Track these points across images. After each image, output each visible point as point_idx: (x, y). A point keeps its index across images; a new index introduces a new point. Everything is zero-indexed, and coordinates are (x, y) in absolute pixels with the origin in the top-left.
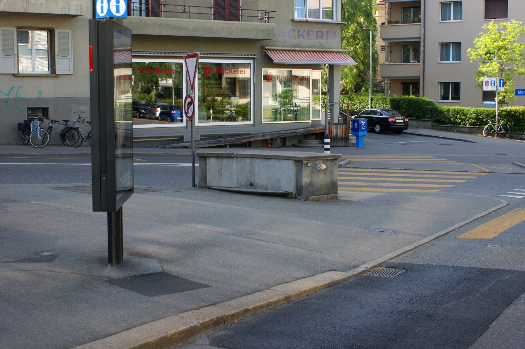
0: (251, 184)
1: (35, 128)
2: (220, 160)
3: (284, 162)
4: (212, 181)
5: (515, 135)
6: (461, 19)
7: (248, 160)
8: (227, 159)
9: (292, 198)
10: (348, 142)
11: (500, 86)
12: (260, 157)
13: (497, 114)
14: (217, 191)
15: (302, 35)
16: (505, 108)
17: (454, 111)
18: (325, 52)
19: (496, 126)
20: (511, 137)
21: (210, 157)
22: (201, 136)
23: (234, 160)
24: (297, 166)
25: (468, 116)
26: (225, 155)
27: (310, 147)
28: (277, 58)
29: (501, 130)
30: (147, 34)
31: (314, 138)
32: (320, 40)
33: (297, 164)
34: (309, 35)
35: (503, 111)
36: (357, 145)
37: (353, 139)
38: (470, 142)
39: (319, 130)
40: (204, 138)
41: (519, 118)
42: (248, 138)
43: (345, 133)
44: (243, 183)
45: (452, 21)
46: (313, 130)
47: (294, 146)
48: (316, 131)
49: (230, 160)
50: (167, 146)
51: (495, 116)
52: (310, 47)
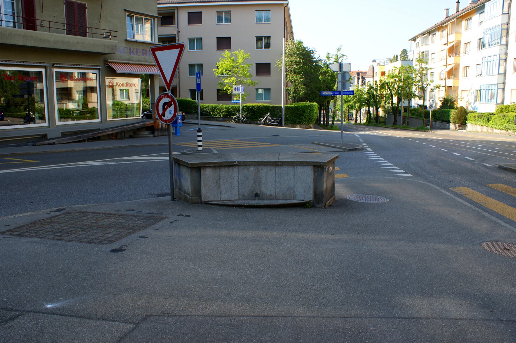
0: (257, 195)
2: (217, 170)
3: (299, 169)
6: (202, 49)
7: (252, 169)
8: (227, 169)
9: (311, 207)
15: (132, 52)
16: (245, 105)
17: (212, 107)
18: (149, 65)
20: (250, 123)
21: (205, 167)
22: (62, 133)
23: (235, 169)
24: (315, 172)
26: (225, 164)
28: (119, 69)
29: (244, 118)
30: (12, 43)
32: (144, 56)
34: (137, 52)
36: (176, 134)
37: (173, 130)
40: (65, 135)
42: (101, 133)
44: (246, 194)
45: (196, 50)
47: (131, 137)
50: (37, 144)
52: (138, 61)
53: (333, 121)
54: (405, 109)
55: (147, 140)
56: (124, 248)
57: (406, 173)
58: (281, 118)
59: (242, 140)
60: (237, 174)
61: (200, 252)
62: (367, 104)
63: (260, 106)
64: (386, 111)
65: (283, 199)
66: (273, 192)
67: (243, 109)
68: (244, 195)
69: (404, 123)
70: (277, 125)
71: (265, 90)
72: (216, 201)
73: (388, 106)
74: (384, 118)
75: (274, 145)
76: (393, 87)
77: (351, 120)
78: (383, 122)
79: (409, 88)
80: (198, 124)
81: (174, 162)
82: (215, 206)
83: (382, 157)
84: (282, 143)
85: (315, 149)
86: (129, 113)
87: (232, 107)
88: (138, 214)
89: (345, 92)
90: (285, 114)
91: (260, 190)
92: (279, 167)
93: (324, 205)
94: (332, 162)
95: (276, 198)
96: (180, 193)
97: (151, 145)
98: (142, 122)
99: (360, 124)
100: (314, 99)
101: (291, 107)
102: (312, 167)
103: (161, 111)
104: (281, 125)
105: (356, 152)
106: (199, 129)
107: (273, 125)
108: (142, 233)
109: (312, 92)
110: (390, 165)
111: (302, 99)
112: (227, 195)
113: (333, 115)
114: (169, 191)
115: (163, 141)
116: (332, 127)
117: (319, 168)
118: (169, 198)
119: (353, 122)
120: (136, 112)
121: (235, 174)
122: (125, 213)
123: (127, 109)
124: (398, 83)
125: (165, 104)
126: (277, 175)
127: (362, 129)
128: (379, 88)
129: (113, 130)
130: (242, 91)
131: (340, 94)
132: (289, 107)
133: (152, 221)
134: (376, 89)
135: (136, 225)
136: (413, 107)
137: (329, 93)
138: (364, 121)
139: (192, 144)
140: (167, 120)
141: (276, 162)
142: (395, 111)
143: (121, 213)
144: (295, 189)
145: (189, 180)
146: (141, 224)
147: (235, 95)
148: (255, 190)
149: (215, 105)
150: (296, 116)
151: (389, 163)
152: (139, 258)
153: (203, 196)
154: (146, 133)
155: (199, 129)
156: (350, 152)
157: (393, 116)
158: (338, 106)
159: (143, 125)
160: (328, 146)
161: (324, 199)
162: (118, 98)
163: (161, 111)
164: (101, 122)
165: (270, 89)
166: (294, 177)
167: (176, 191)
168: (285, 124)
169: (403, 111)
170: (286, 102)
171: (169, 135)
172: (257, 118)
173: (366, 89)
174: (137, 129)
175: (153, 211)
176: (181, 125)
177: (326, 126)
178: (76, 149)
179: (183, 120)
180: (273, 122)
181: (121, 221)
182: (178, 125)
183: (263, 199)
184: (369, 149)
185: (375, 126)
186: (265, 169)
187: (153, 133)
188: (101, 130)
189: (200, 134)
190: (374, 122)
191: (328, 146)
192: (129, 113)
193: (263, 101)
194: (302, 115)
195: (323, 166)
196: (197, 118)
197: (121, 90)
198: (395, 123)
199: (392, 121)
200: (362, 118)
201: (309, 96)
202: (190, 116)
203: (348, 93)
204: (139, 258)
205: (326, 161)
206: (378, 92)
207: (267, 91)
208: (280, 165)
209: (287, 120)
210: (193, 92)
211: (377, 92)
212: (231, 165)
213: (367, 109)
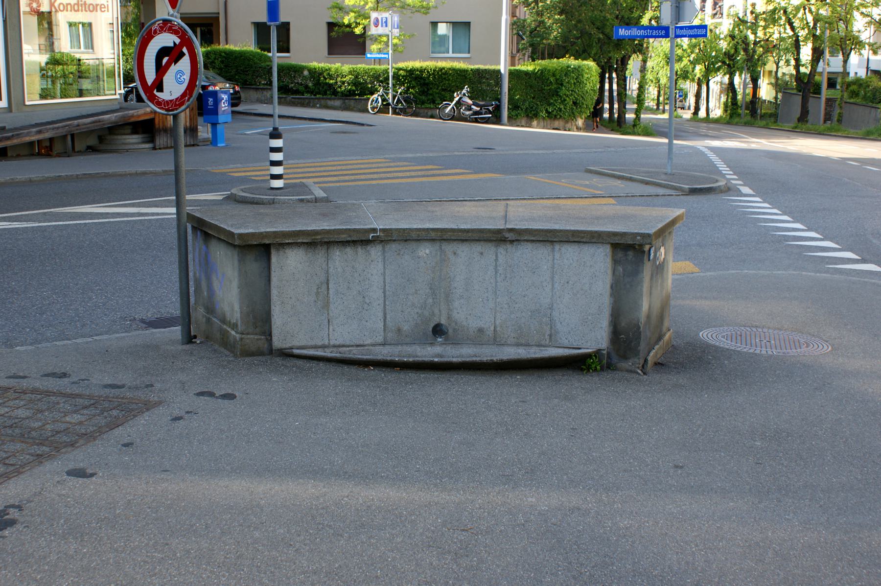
0: (438, 330)
2: (321, 253)
3: (569, 253)
4: (291, 327)
5: (422, 111)
7: (425, 251)
8: (349, 250)
9: (602, 369)
10: (197, 136)
11: (705, 36)
12: (476, 236)
13: (391, 74)
16: (401, 65)
19: (390, 96)
21: (282, 245)
23: (375, 251)
24: (615, 262)
25: (339, 79)
26: (344, 237)
27: (127, 151)
29: (399, 101)
31: (129, 131)
33: (620, 254)
35: (401, 69)
36: (214, 141)
38: (363, 125)
39: (145, 114)
41: (427, 81)
42: (8, 138)
43: (190, 119)
44: (406, 327)
46: (133, 116)
47: (92, 149)
48: (139, 116)
49: (359, 249)
51: (387, 79)
53: (637, 112)
54: (829, 79)
55: (137, 159)
56: (13, 514)
57: (864, 261)
58: (499, 100)
59: (394, 160)
61: (257, 534)
62: (729, 65)
63: (441, 69)
64: (779, 85)
65: (518, 345)
66: (486, 322)
67: (396, 76)
68: (399, 330)
69: (828, 117)
70: (487, 121)
71: (455, 24)
72: (315, 347)
73: (787, 70)
74: (775, 104)
75: (481, 176)
76: (802, 20)
77: (683, 108)
78: (771, 115)
79: (847, 22)
80: (271, 116)
81: (193, 228)
82: (314, 364)
83: (785, 213)
84: (504, 171)
85: (597, 188)
86: (86, 84)
87: (366, 72)
88: (76, 390)
89: (681, 28)
90: (509, 90)
91: (449, 317)
92: (509, 246)
93: (642, 361)
94: (664, 232)
95: (496, 341)
96: (208, 320)
97: (144, 174)
98: (121, 109)
99: (707, 119)
100: (584, 51)
101: (526, 73)
102: (608, 249)
103: (150, 75)
104: (497, 120)
105: (711, 197)
106: (275, 129)
107: (476, 121)
108: (77, 458)
109: (583, 33)
110: (812, 238)
111: (555, 52)
112: (353, 327)
113: (639, 96)
114: (174, 309)
115: (162, 162)
116: (635, 128)
117: (631, 252)
118: (176, 332)
119: (687, 115)
120: (106, 84)
121: (372, 264)
122: (37, 384)
123: (81, 75)
124: (813, 8)
125: (163, 52)
127: (711, 133)
128: (762, 23)
129: (40, 132)
130: (393, 27)
131: (667, 36)
132: (519, 72)
133: (115, 413)
134: (754, 27)
135: (63, 426)
136: (852, 75)
137: (634, 32)
138: (717, 112)
139: (256, 171)
140: (168, 102)
141: (499, 231)
142: (806, 86)
143: (24, 383)
144: (555, 314)
145: (235, 284)
146: (81, 423)
147: (376, 39)
148: (433, 314)
149: (322, 65)
150: (539, 98)
151: (809, 229)
152: (53, 557)
153: (275, 332)
154: (134, 139)
155: (275, 129)
157: (798, 99)
158: (653, 68)
159: (123, 117)
160: (631, 179)
161: (643, 346)
162: (64, 44)
163: (150, 75)
164: (10, 109)
165: (468, 24)
166: (552, 278)
167: (199, 314)
168: (509, 117)
169: (825, 85)
170: (513, 60)
171: (175, 147)
172: (434, 102)
173: (725, 26)
174: (109, 128)
175: (125, 378)
176: (229, 118)
177: (618, 125)
179: (233, 105)
180: (476, 113)
181: (22, 413)
182: (221, 118)
183: (456, 343)
184: (746, 190)
185: (746, 124)
186: (465, 251)
187: (152, 140)
188: (11, 130)
189: (277, 143)
190: (745, 113)
191: (631, 179)
192: (86, 84)
193: (451, 54)
194: (556, 93)
195: (641, 246)
196: (270, 101)
197: (71, 25)
198: (803, 117)
199: (797, 112)
200: (711, 105)
201: (573, 44)
202: (253, 95)
203: (691, 32)
204: (53, 557)
205: (652, 231)
206: (760, 34)
207: (462, 27)
208: (512, 242)
209: (514, 106)
210: (262, 31)
211: (755, 34)
212: (361, 240)
213: (726, 79)
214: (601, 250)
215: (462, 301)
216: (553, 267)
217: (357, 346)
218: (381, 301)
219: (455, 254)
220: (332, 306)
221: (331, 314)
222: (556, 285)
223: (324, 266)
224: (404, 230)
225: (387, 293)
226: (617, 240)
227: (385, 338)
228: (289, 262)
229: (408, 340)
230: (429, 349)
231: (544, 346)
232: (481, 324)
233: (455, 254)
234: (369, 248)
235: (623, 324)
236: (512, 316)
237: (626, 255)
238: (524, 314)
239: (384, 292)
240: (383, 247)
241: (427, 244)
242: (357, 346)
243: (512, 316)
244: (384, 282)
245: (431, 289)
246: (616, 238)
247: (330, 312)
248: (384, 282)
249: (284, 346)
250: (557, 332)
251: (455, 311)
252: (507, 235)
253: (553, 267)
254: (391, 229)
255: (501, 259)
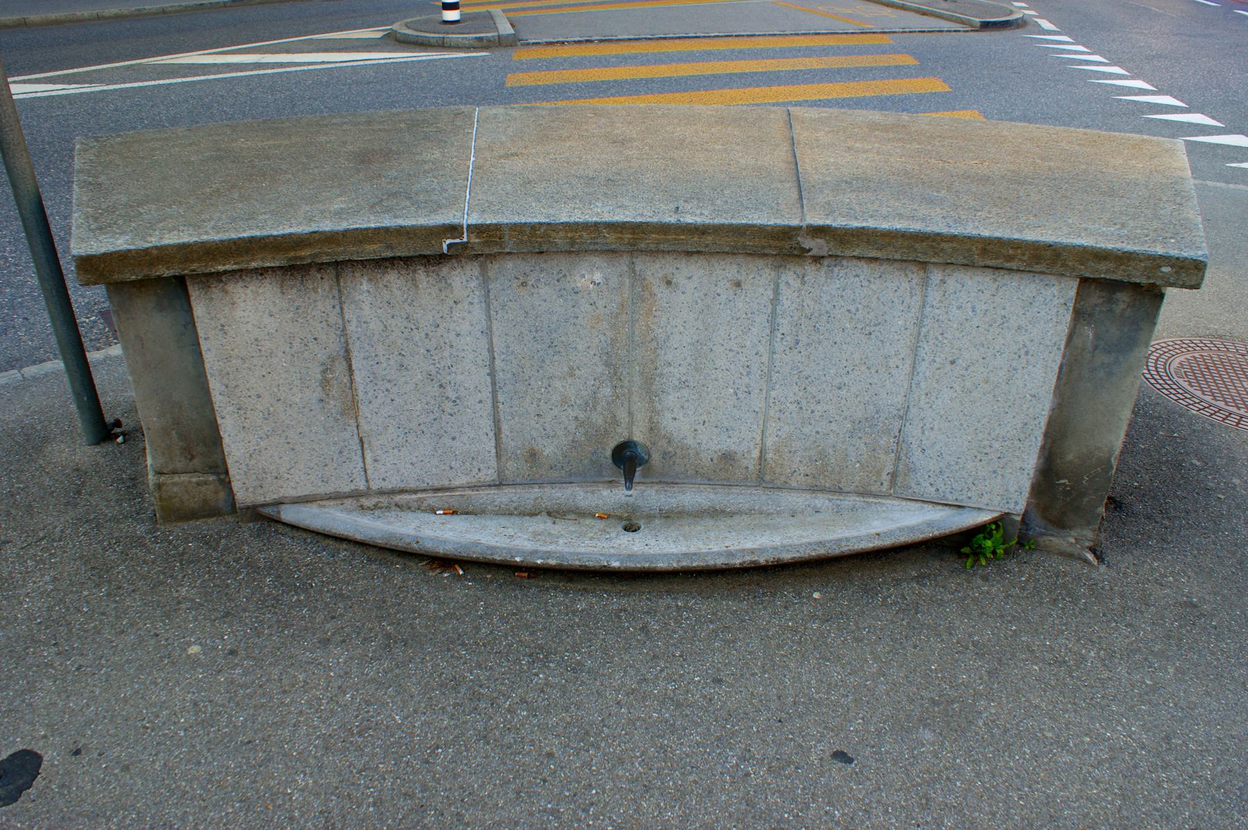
0: (627, 460)
1: (3, 387)
2: (319, 298)
3: (967, 295)
7: (592, 275)
8: (394, 279)
14: (907, 586)
23: (462, 279)
24: (1079, 315)
26: (372, 250)
33: (1095, 298)
44: (549, 450)
49: (421, 275)
60: (478, 312)
68: (533, 455)
91: (653, 428)
105: (1007, 33)
117: (1120, 291)
121: (455, 308)
126: (785, 325)
141: (787, 233)
144: (913, 431)
148: (615, 421)
156: (986, 36)
166: (915, 350)
178: (34, 17)
183: (668, 481)
184: (1046, 24)
208: (817, 259)
214: (1055, 290)
215: (685, 392)
216: (919, 323)
217: (437, 490)
218: (486, 394)
219: (669, 283)
220: (364, 410)
221: (365, 427)
222: (923, 367)
223: (334, 318)
224: (534, 227)
225: (500, 376)
226: (1103, 271)
227: (500, 472)
228: (239, 313)
229: (555, 474)
230: (606, 493)
231: (876, 496)
232: (729, 444)
233: (669, 283)
234: (445, 270)
235: (1070, 457)
236: (806, 430)
237: (1110, 301)
238: (834, 426)
239: (492, 374)
240: (483, 268)
241: (598, 260)
242: (437, 490)
243: (806, 430)
244: (491, 350)
245: (607, 364)
246: (1103, 266)
247: (362, 421)
248: (491, 350)
249: (261, 499)
250: (910, 470)
251: (668, 415)
252: (808, 243)
253: (919, 323)
254: (498, 227)
255: (788, 298)
